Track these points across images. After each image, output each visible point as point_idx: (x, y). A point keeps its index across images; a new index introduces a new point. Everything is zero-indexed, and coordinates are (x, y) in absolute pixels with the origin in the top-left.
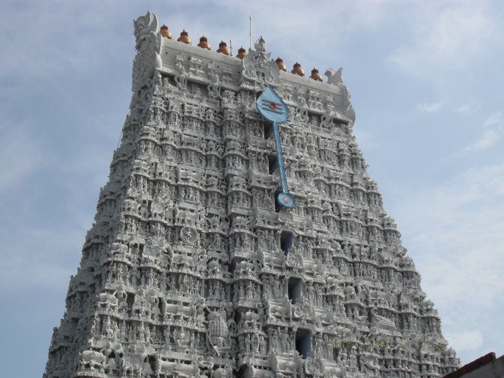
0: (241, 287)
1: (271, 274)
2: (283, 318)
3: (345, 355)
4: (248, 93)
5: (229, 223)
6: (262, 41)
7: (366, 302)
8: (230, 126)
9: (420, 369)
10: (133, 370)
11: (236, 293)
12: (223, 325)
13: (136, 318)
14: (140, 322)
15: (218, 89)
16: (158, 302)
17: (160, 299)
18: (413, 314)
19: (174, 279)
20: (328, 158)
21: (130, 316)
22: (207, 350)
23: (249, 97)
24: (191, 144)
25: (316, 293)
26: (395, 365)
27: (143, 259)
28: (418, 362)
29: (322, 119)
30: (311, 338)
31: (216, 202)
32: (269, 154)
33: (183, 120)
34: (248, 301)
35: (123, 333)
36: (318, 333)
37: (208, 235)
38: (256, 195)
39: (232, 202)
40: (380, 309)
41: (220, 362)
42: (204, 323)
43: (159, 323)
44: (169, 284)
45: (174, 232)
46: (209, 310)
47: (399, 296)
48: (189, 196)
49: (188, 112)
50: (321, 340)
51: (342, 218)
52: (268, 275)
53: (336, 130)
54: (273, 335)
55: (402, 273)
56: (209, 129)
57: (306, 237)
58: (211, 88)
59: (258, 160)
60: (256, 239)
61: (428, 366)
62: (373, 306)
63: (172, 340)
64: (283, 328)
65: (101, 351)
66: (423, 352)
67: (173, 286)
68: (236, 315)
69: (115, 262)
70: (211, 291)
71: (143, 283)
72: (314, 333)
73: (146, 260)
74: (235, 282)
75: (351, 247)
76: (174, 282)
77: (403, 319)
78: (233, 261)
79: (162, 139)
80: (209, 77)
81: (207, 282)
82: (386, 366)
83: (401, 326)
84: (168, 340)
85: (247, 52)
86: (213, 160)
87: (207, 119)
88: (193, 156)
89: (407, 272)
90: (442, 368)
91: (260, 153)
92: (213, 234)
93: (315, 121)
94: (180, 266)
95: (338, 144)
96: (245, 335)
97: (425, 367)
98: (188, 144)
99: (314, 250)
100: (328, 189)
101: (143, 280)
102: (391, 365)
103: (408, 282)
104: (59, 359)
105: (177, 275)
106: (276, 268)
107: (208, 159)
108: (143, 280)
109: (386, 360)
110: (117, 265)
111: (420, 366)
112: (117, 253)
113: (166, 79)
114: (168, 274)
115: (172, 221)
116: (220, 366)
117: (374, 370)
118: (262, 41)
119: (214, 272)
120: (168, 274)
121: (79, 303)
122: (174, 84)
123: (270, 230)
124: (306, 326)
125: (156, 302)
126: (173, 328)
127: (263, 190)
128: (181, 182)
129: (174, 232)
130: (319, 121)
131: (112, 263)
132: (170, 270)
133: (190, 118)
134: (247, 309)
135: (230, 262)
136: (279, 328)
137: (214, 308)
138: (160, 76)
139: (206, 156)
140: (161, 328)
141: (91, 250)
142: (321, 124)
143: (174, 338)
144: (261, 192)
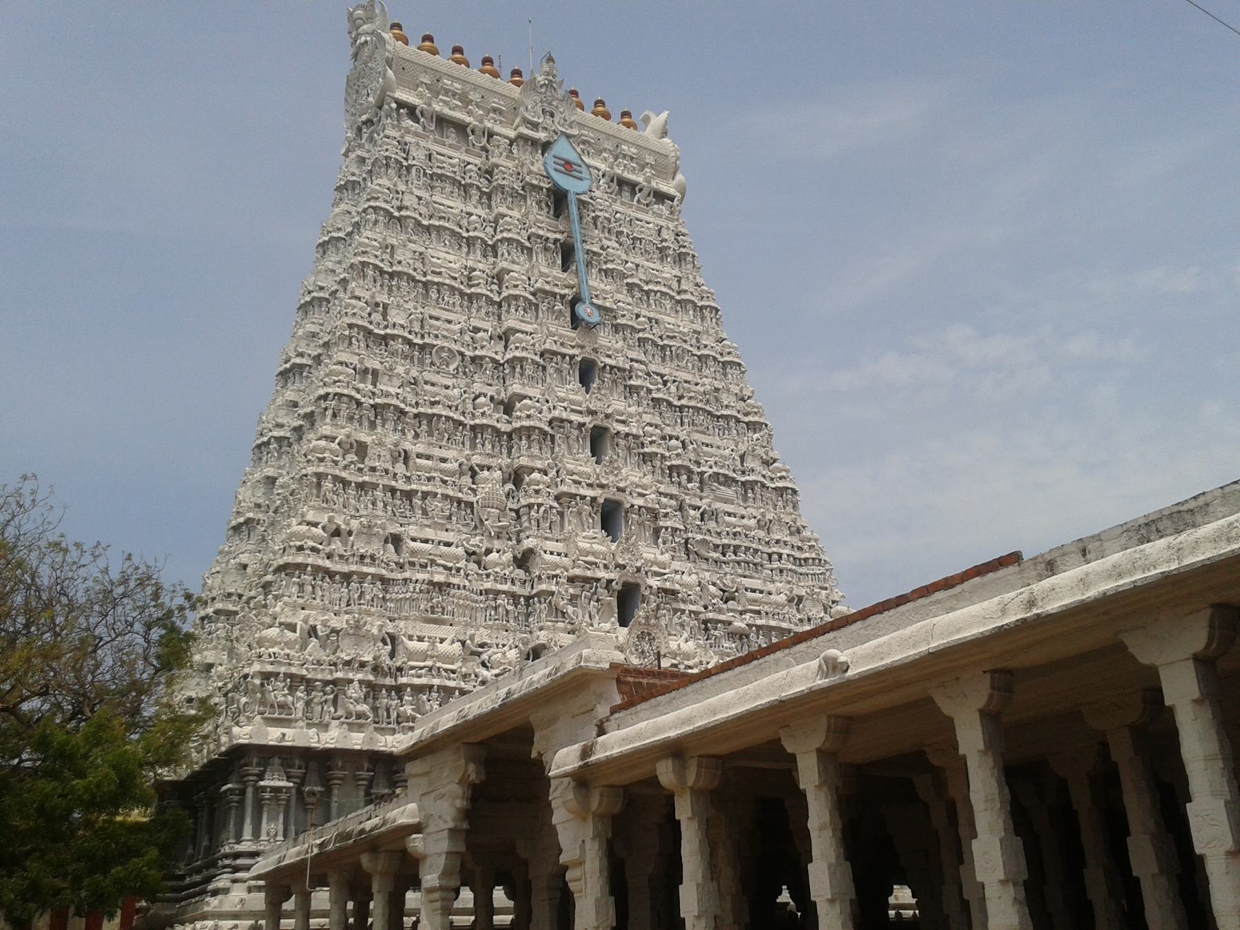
5: (503, 343)
17: (405, 451)
23: (530, 149)
37: (473, 359)
39: (508, 312)
61: (780, 555)
69: (335, 394)
76: (424, 427)
79: (400, 209)
81: (473, 428)
89: (755, 423)
92: (482, 358)
93: (626, 194)
97: (776, 557)
101: (378, 422)
103: (755, 436)
123: (564, 356)
124: (619, 496)
126: (425, 495)
127: (554, 295)
130: (633, 193)
138: (394, 105)
139: (467, 239)
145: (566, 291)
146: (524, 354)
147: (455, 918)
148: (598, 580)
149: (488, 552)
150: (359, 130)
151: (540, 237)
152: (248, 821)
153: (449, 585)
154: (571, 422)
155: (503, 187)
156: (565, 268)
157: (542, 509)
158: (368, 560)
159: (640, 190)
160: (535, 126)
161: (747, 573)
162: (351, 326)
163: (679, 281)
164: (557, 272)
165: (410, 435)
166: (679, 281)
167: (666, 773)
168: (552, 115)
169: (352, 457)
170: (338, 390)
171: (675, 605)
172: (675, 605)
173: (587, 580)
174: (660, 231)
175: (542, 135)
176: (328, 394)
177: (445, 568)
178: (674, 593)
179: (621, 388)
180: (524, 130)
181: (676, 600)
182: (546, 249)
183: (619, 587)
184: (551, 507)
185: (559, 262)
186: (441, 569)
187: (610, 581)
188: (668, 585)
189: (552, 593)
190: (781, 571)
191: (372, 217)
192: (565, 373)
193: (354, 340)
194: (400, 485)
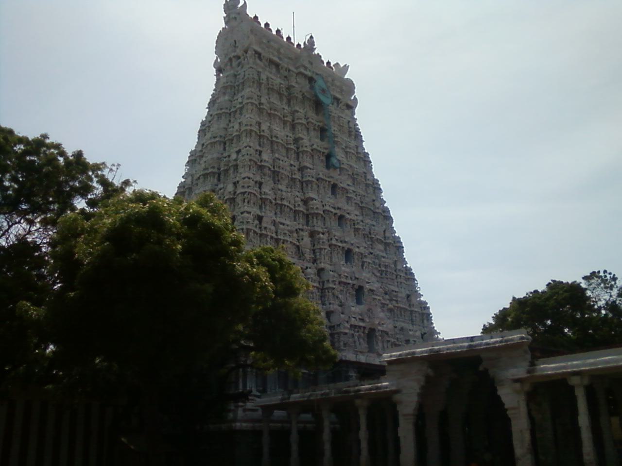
0: (315, 218)
5: (301, 172)
6: (311, 37)
7: (370, 233)
8: (296, 100)
12: (307, 240)
13: (266, 233)
14: (268, 235)
15: (267, 60)
18: (322, 215)
19: (279, 207)
21: (261, 231)
22: (300, 257)
25: (350, 226)
26: (386, 274)
27: (263, 193)
28: (395, 273)
29: (340, 102)
33: (268, 90)
34: (319, 226)
36: (356, 252)
40: (378, 239)
41: (309, 265)
45: (276, 175)
50: (357, 257)
53: (347, 111)
59: (314, 129)
60: (318, 186)
61: (401, 276)
62: (373, 236)
64: (340, 247)
67: (279, 213)
68: (312, 234)
69: (249, 193)
70: (297, 217)
72: (355, 251)
73: (265, 194)
74: (310, 214)
76: (279, 209)
77: (387, 245)
80: (279, 58)
82: (381, 274)
83: (385, 249)
85: (302, 46)
86: (288, 124)
91: (315, 124)
92: (295, 179)
94: (282, 199)
96: (321, 249)
102: (384, 274)
105: (281, 205)
106: (332, 207)
107: (285, 123)
111: (396, 276)
113: (257, 56)
114: (276, 204)
118: (311, 37)
122: (261, 60)
124: (351, 247)
127: (320, 152)
129: (276, 175)
130: (338, 104)
131: (247, 193)
133: (272, 89)
145: (325, 151)
147: (271, 424)
148: (349, 284)
149: (307, 268)
150: (230, 60)
151: (312, 123)
152: (241, 380)
154: (332, 212)
155: (297, 97)
156: (322, 139)
157: (326, 250)
159: (341, 102)
160: (306, 68)
162: (250, 160)
164: (318, 140)
167: (574, 381)
169: (257, 222)
170: (250, 191)
171: (373, 296)
172: (373, 296)
175: (309, 74)
176: (246, 192)
179: (345, 197)
180: (302, 70)
181: (374, 294)
182: (314, 129)
183: (357, 288)
187: (354, 285)
188: (372, 288)
189: (334, 289)
190: (401, 283)
191: (250, 107)
192: (326, 189)
193: (251, 167)
194: (274, 235)
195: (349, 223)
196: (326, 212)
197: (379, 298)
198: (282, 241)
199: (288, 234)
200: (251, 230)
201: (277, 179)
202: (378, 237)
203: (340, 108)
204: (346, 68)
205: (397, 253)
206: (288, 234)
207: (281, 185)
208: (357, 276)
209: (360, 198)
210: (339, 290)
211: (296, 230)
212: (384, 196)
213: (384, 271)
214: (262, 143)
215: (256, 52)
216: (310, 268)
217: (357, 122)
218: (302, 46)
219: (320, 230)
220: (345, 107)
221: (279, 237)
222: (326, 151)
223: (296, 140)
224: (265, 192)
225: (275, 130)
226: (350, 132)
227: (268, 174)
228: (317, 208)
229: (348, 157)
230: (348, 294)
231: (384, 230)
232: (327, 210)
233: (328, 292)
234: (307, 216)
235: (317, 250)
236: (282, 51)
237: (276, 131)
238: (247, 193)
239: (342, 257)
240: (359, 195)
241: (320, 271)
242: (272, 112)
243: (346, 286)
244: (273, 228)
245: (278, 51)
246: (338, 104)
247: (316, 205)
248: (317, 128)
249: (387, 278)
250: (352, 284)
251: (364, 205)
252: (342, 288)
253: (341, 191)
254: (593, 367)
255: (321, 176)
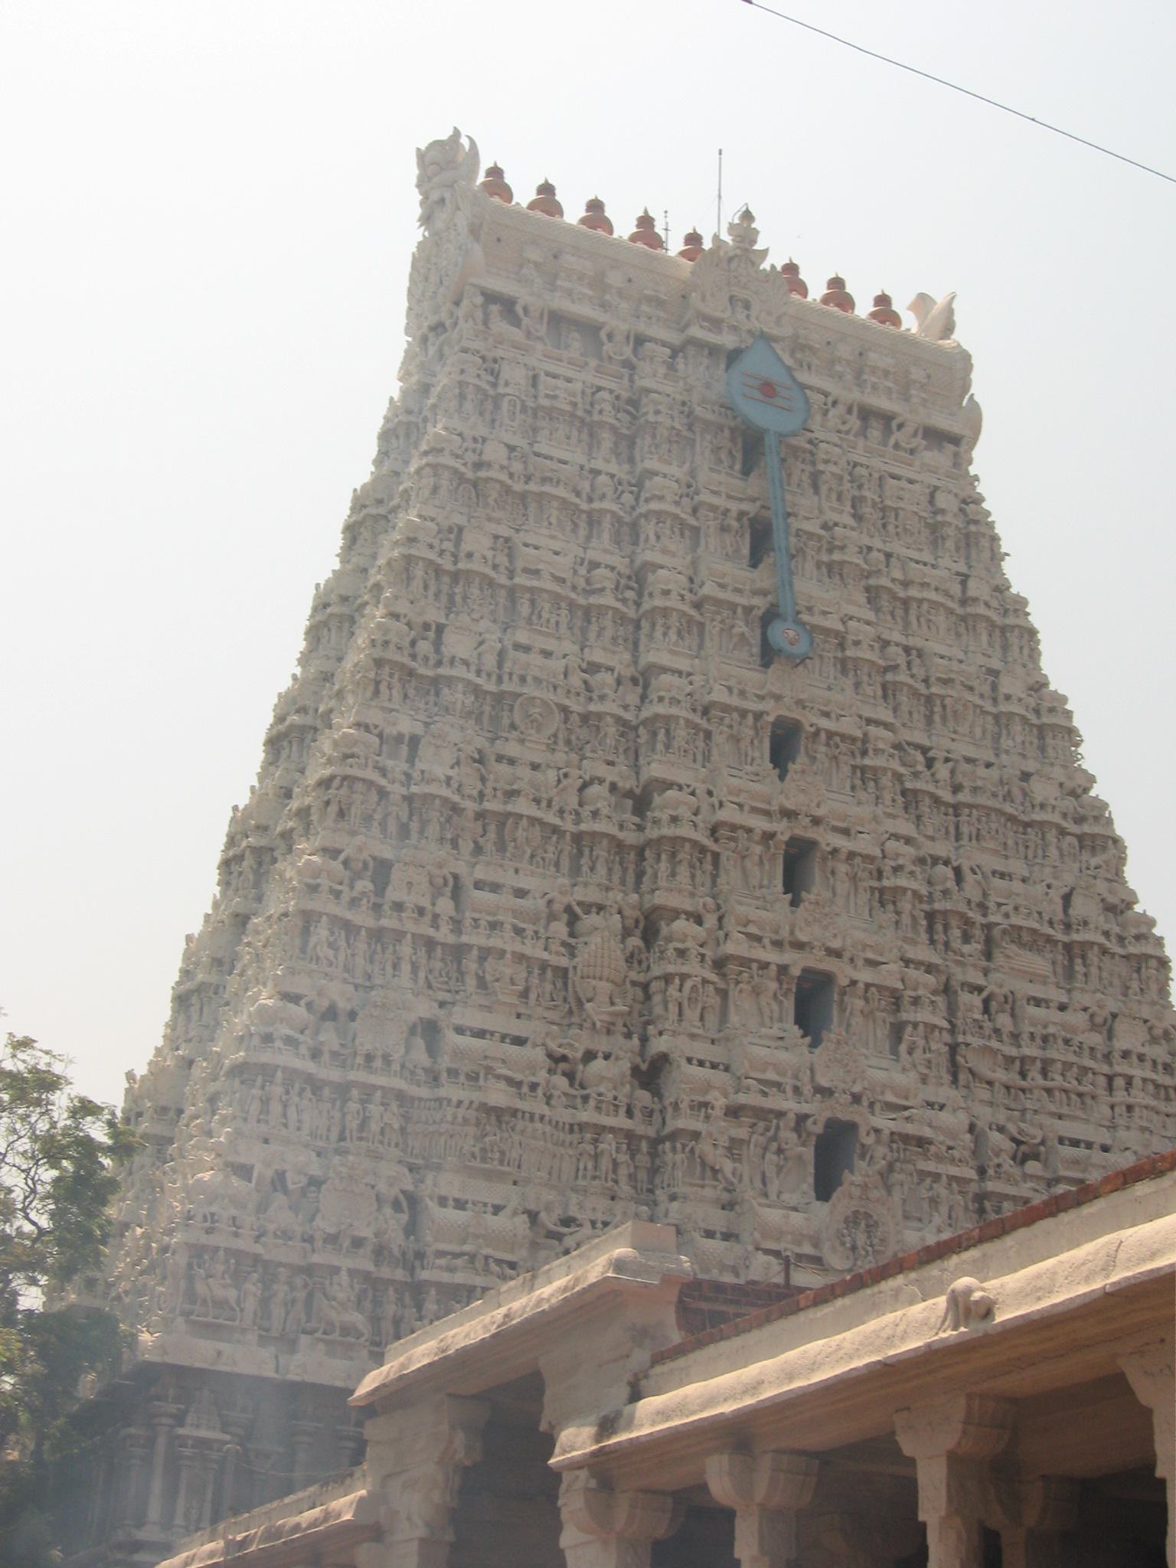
1: (742, 827)
2: (766, 941)
3: (921, 1043)
4: (706, 352)
6: (747, 216)
7: (983, 908)
8: (654, 437)
9: (1110, 1088)
10: (379, 1053)
11: (649, 871)
16: (451, 882)
17: (456, 877)
19: (492, 827)
20: (905, 530)
24: (551, 479)
25: (854, 879)
26: (1044, 1073)
27: (416, 775)
30: (836, 997)
31: (609, 633)
32: (751, 515)
33: (535, 416)
35: (360, 961)
37: (585, 718)
38: (713, 620)
39: (651, 637)
41: (602, 1044)
42: (564, 944)
43: (451, 939)
44: (481, 840)
46: (578, 910)
47: (1067, 899)
48: (540, 617)
49: (547, 396)
51: (517, 580)
52: (734, 828)
54: (738, 983)
55: (1080, 838)
56: (599, 443)
57: (836, 734)
58: (610, 336)
63: (482, 984)
65: (303, 1002)
66: (1121, 1043)
71: (414, 835)
74: (649, 843)
75: (951, 764)
76: (492, 835)
78: (645, 788)
81: (577, 838)
82: (1023, 1075)
84: (471, 983)
87: (596, 417)
88: (555, 512)
90: (1166, 1088)
92: (600, 716)
95: (932, 496)
96: (667, 979)
98: (545, 480)
99: (854, 767)
100: (899, 612)
101: (414, 826)
102: (1034, 1073)
103: (1094, 862)
104: (195, 1016)
108: (414, 826)
109: (1023, 1060)
110: (350, 787)
111: (1110, 1079)
112: (352, 756)
113: (494, 309)
115: (494, 678)
116: (600, 1054)
117: (990, 1083)
118: (747, 216)
119: (595, 814)
120: (480, 815)
121: (251, 877)
124: (829, 965)
125: (446, 884)
126: (485, 953)
127: (733, 607)
128: (521, 580)
130: (887, 431)
132: (488, 805)
134: (676, 914)
135: (638, 791)
136: (755, 966)
137: (591, 905)
140: (459, 951)
141: (285, 744)
142: (892, 441)
143: (488, 978)
144: (726, 613)
145: (757, 601)
146: (674, 711)
148: (780, 1114)
149: (589, 1056)
151: (713, 508)
153: (514, 1113)
154: (749, 831)
157: (689, 984)
158: (378, 1063)
159: (900, 426)
160: (716, 324)
161: (1065, 1110)
163: (964, 583)
165: (466, 847)
166: (964, 583)
168: (747, 306)
171: (923, 1165)
173: (761, 1113)
174: (932, 496)
177: (510, 1081)
178: (922, 1142)
180: (696, 332)
183: (819, 1129)
184: (705, 981)
185: (746, 550)
186: (502, 1085)
187: (802, 1118)
188: (910, 1129)
189: (696, 1135)
190: (1130, 1108)
195: (842, 868)
196: (723, 832)
197: (954, 1171)
198: (475, 952)
199: (508, 927)
200: (1053, 1061)
201: (506, 721)
202: (1015, 920)
203: (897, 446)
204: (745, 226)
205: (1135, 985)
206: (508, 927)
207: (522, 741)
208: (824, 1082)
209: (953, 772)
210: (724, 1141)
211: (568, 909)
212: (1091, 757)
213: (1034, 1059)
214: (458, 599)
215: (490, 297)
216: (607, 1057)
217: (980, 489)
218: (707, 245)
219: (675, 901)
220: (919, 441)
221: (465, 939)
222: (761, 603)
223: (638, 579)
224: (423, 772)
225: (526, 545)
226: (934, 528)
227: (459, 706)
228: (674, 819)
229: (913, 619)
230: (771, 1157)
231: (1066, 890)
232: (722, 824)
233: (674, 1150)
234: (640, 852)
235: (655, 986)
236: (615, 279)
237: (531, 551)
238: (336, 783)
239: (775, 1007)
240: (947, 760)
241: (651, 1074)
242: (532, 487)
243: (762, 1124)
244: (445, 906)
245: (598, 282)
246: (887, 431)
247: (676, 815)
248: (735, 524)
249: (1049, 1091)
250: (791, 1116)
251: (964, 797)
252: (741, 1133)
253: (823, 749)
254: (749, 1401)
255: (719, 695)
